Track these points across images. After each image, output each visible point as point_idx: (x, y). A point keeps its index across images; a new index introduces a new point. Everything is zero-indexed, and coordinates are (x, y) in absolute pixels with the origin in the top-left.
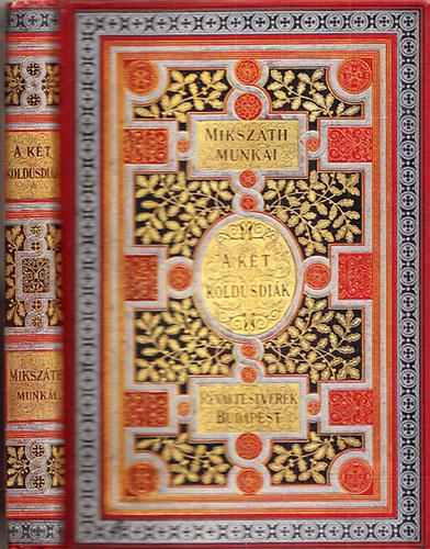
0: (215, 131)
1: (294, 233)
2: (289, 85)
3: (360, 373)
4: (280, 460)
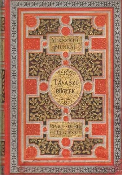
0: (58, 46)
1: (51, 101)
2: (52, 149)
3: (102, 118)
4: (76, 146)
